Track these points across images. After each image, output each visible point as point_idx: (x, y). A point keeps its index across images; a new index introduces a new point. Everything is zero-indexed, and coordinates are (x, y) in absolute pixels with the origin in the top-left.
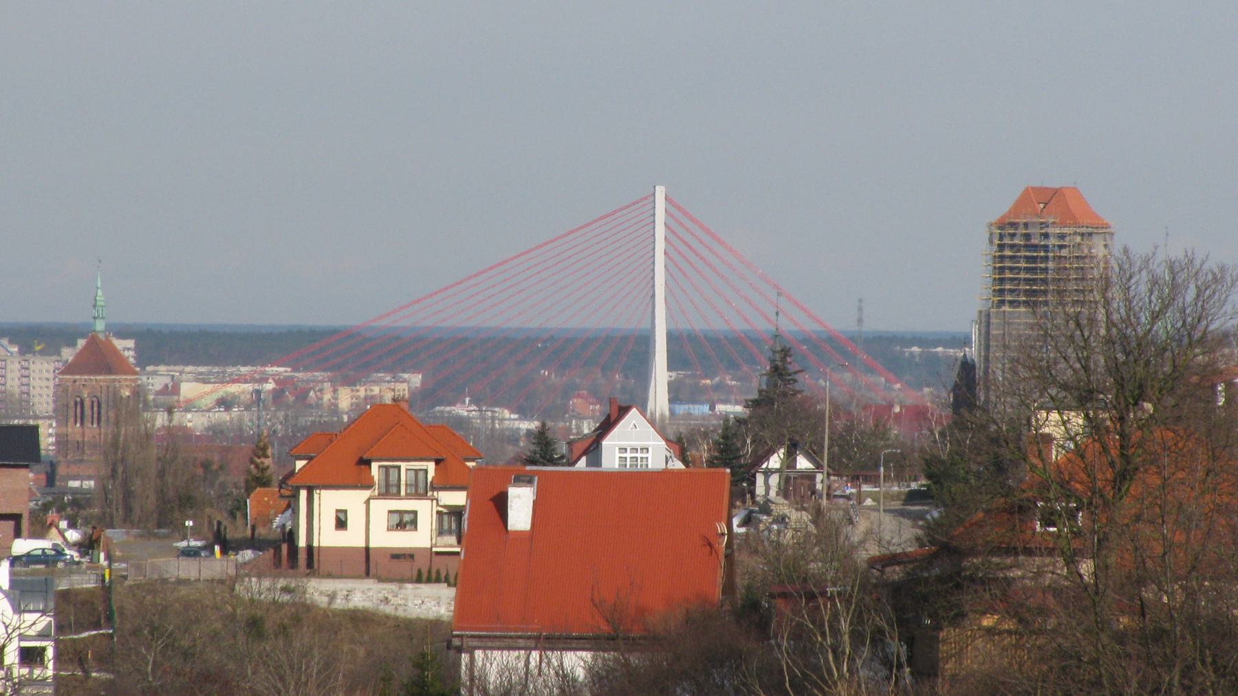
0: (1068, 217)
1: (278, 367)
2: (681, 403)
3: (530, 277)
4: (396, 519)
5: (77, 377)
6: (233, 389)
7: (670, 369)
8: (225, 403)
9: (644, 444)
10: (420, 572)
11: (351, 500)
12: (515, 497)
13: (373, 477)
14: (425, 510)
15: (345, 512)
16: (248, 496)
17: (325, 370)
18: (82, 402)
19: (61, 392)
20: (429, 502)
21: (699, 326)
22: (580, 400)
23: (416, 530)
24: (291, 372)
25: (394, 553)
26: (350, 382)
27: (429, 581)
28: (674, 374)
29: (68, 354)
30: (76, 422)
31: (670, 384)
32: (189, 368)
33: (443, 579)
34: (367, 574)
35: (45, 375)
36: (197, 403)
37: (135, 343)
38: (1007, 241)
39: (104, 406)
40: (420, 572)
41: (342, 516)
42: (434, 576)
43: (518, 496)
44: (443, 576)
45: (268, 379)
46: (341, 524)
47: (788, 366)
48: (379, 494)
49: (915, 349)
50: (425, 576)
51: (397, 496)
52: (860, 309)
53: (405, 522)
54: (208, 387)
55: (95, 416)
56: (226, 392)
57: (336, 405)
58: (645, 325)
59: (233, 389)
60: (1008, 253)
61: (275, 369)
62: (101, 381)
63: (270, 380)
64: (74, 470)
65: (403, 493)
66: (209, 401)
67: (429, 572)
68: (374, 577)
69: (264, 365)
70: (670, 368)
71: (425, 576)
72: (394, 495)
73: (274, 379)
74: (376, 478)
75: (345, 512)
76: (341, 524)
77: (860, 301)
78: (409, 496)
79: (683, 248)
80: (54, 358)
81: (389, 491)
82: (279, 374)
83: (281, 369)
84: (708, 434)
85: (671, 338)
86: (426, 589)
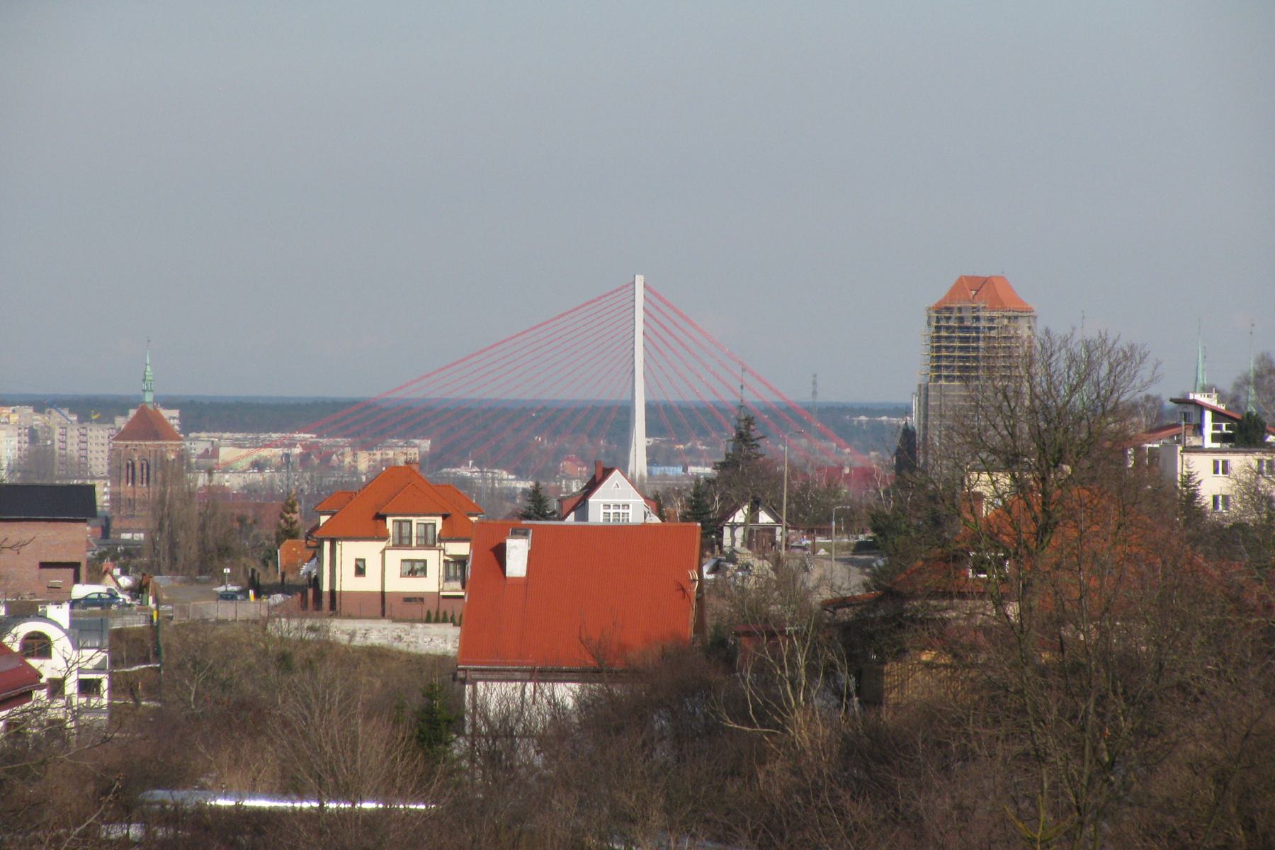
1: (305, 433)
4: (408, 567)
5: (129, 442)
6: (265, 453)
7: (648, 435)
8: (258, 465)
11: (369, 550)
12: (512, 548)
14: (434, 559)
15: (363, 561)
16: (279, 547)
17: (345, 436)
18: (133, 465)
19: (114, 456)
21: (673, 397)
25: (406, 596)
26: (368, 447)
27: (437, 621)
28: (651, 440)
29: (121, 422)
31: (648, 449)
32: (227, 435)
33: (449, 619)
34: (383, 615)
35: (101, 441)
36: (234, 465)
37: (180, 413)
38: (943, 323)
39: (152, 468)
41: (360, 564)
42: (441, 616)
46: (360, 571)
48: (393, 545)
49: (863, 418)
50: (433, 617)
51: (409, 546)
52: (815, 383)
53: (415, 569)
54: (244, 452)
56: (259, 456)
58: (627, 397)
59: (265, 453)
60: (944, 334)
61: (302, 435)
63: (298, 446)
64: (125, 524)
65: (414, 544)
66: (244, 463)
67: (437, 613)
69: (293, 432)
72: (407, 546)
73: (301, 444)
75: (363, 561)
76: (360, 571)
77: (815, 376)
78: (419, 547)
80: (109, 426)
82: (306, 440)
83: (308, 436)
85: (649, 408)
86: (434, 628)
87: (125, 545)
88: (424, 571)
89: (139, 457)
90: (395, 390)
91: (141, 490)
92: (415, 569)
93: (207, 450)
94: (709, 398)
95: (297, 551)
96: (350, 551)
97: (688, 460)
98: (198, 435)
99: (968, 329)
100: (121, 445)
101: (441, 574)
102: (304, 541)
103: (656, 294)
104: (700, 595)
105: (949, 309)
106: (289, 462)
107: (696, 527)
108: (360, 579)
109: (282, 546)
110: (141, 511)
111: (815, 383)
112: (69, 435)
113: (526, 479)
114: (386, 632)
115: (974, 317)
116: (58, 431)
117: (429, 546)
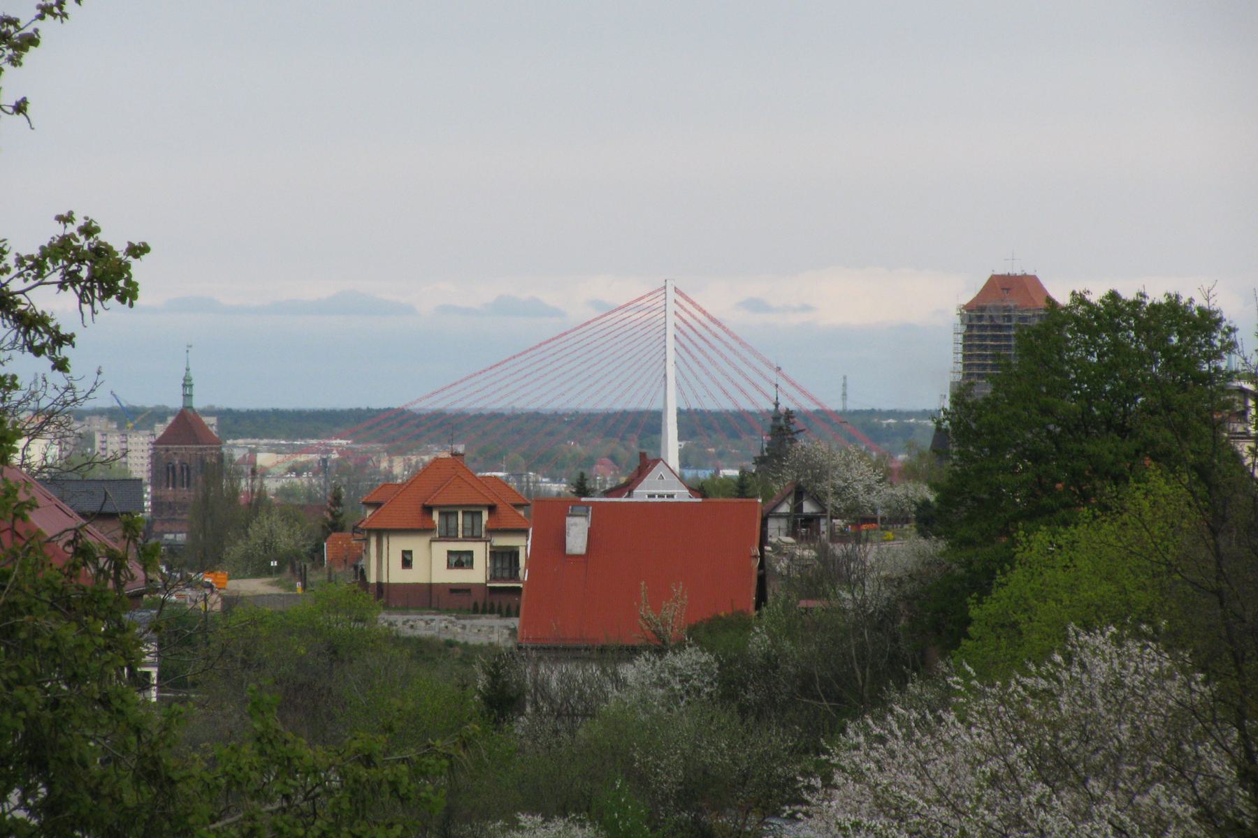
0: (789, 531)
1: (341, 439)
2: (689, 469)
3: (527, 384)
4: (454, 560)
5: (170, 446)
6: (302, 458)
7: (680, 439)
8: (297, 470)
9: (670, 492)
10: (476, 605)
11: (417, 545)
12: (572, 525)
13: (434, 522)
14: (480, 551)
15: (410, 552)
16: (325, 540)
17: (380, 442)
18: (174, 468)
19: (155, 458)
20: (484, 544)
21: (695, 405)
22: (602, 467)
23: (472, 568)
24: (352, 443)
25: (454, 588)
26: (401, 452)
27: (484, 612)
28: (683, 444)
29: (160, 429)
30: (168, 486)
31: (681, 452)
32: (265, 441)
33: (496, 610)
34: (430, 607)
35: (141, 447)
36: (272, 470)
37: (218, 420)
38: (975, 323)
39: (193, 472)
40: (476, 605)
41: (408, 557)
42: (488, 608)
43: (575, 524)
44: (496, 607)
45: (332, 450)
46: (407, 563)
47: (791, 427)
48: (440, 537)
49: (891, 421)
50: (480, 607)
51: (455, 538)
52: (845, 385)
53: (461, 560)
54: (281, 457)
55: (185, 480)
56: (296, 462)
57: (390, 472)
58: (656, 406)
59: (302, 458)
60: (975, 332)
61: (339, 441)
62: (191, 449)
63: (335, 452)
64: (167, 526)
65: (460, 536)
66: (281, 470)
67: (484, 605)
68: (434, 609)
69: (329, 438)
70: (681, 437)
71: (480, 607)
72: (454, 537)
73: (337, 450)
74: (437, 523)
75: (410, 552)
76: (407, 563)
77: (845, 378)
78: (465, 539)
79: (688, 330)
80: (148, 432)
81: (448, 536)
82: (340, 445)
83: (344, 442)
84: (780, 428)
85: (680, 412)
86: (484, 621)
87: (167, 545)
88: (470, 564)
89: (180, 461)
90: (420, 400)
91: (184, 494)
92: (461, 560)
93: (244, 456)
94: (728, 406)
95: (342, 544)
96: (396, 546)
97: (720, 462)
98: (235, 442)
99: (1000, 328)
100: (161, 450)
101: (488, 565)
102: (350, 534)
103: (444, 506)
104: (762, 571)
105: (982, 309)
106: (326, 467)
107: (757, 502)
108: (407, 571)
109: (330, 539)
110: (182, 514)
111: (845, 385)
112: (108, 442)
113: (560, 482)
114: (433, 624)
115: (1004, 316)
116: (98, 438)
117: (476, 537)
